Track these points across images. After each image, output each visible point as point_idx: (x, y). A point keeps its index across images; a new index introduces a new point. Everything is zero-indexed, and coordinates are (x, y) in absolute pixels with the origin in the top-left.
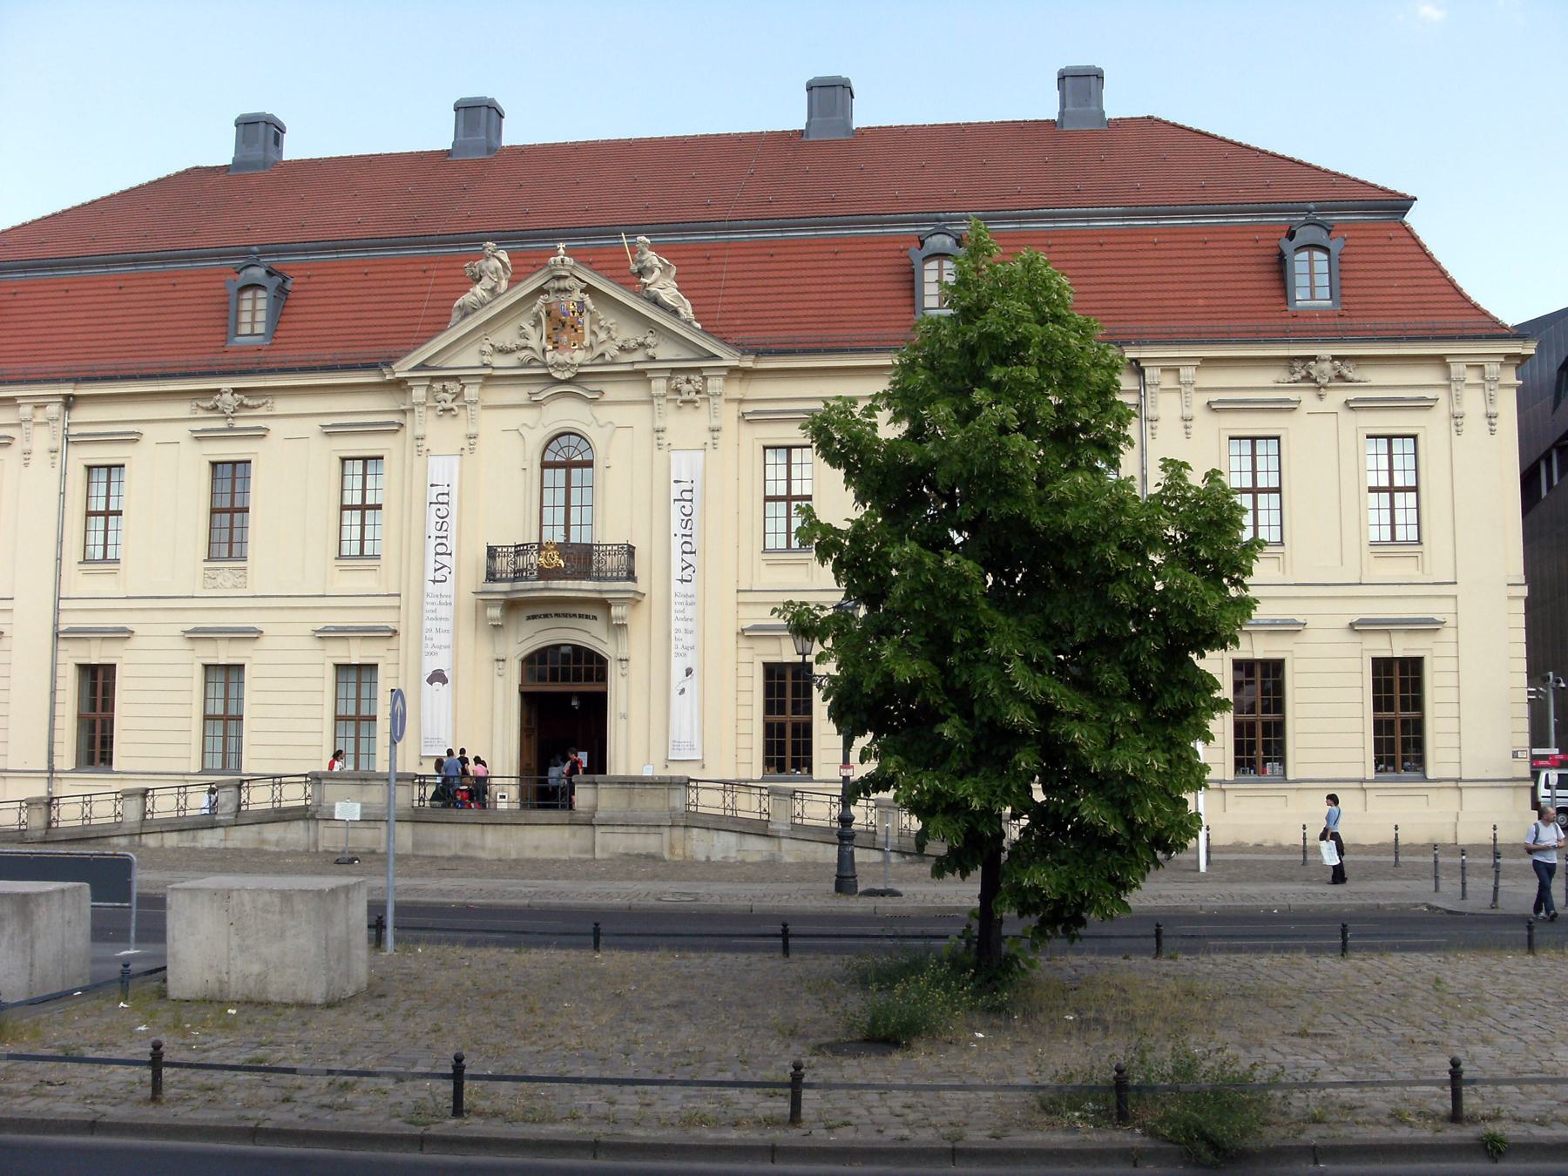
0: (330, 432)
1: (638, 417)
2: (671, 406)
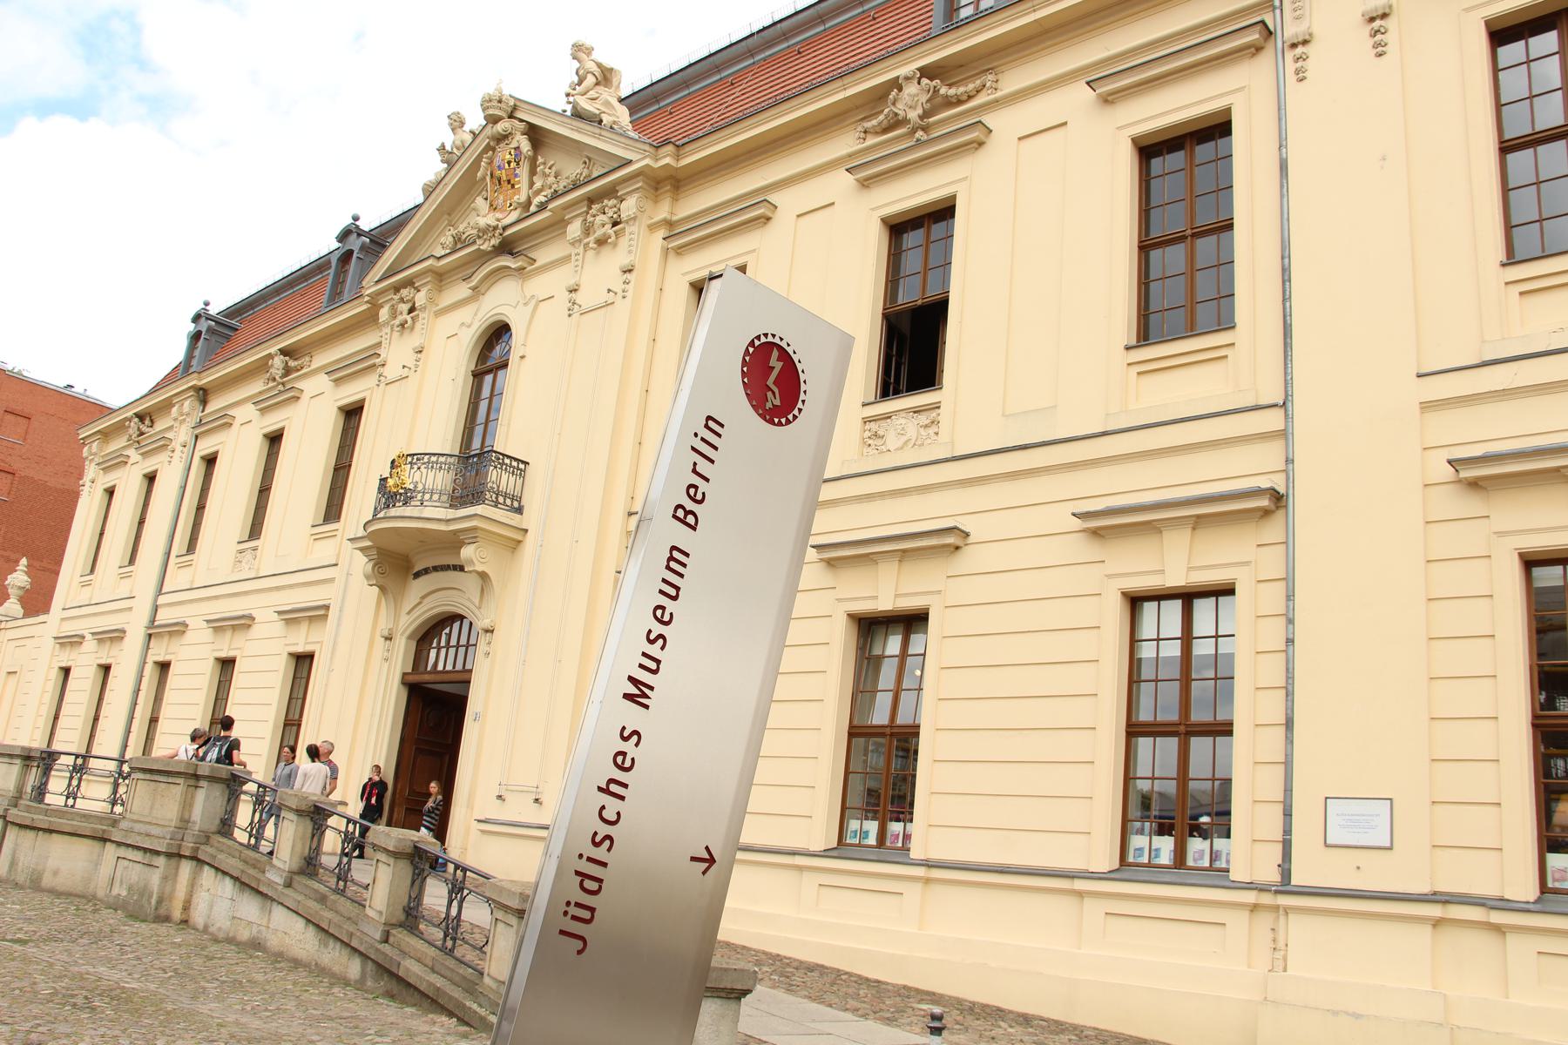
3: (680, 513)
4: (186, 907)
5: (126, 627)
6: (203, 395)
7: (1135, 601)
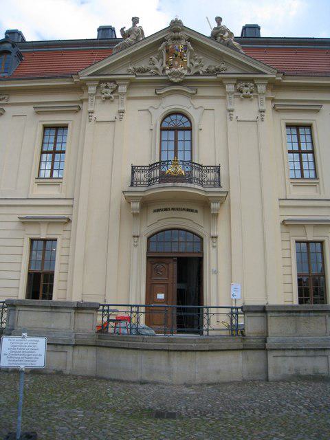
0: (39, 111)
1: (218, 106)
2: (237, 99)
7: (32, 240)
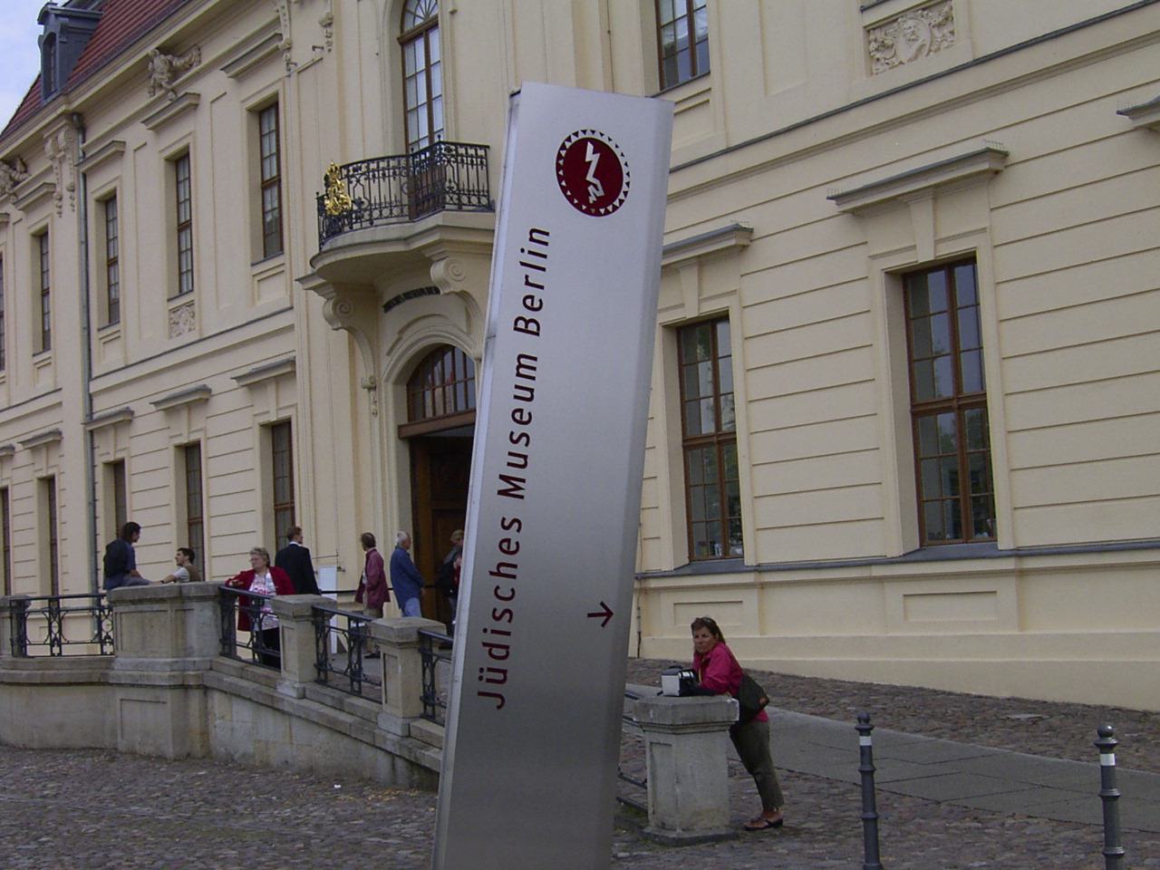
3: (521, 324)
4: (205, 733)
5: (60, 427)
6: (78, 122)
